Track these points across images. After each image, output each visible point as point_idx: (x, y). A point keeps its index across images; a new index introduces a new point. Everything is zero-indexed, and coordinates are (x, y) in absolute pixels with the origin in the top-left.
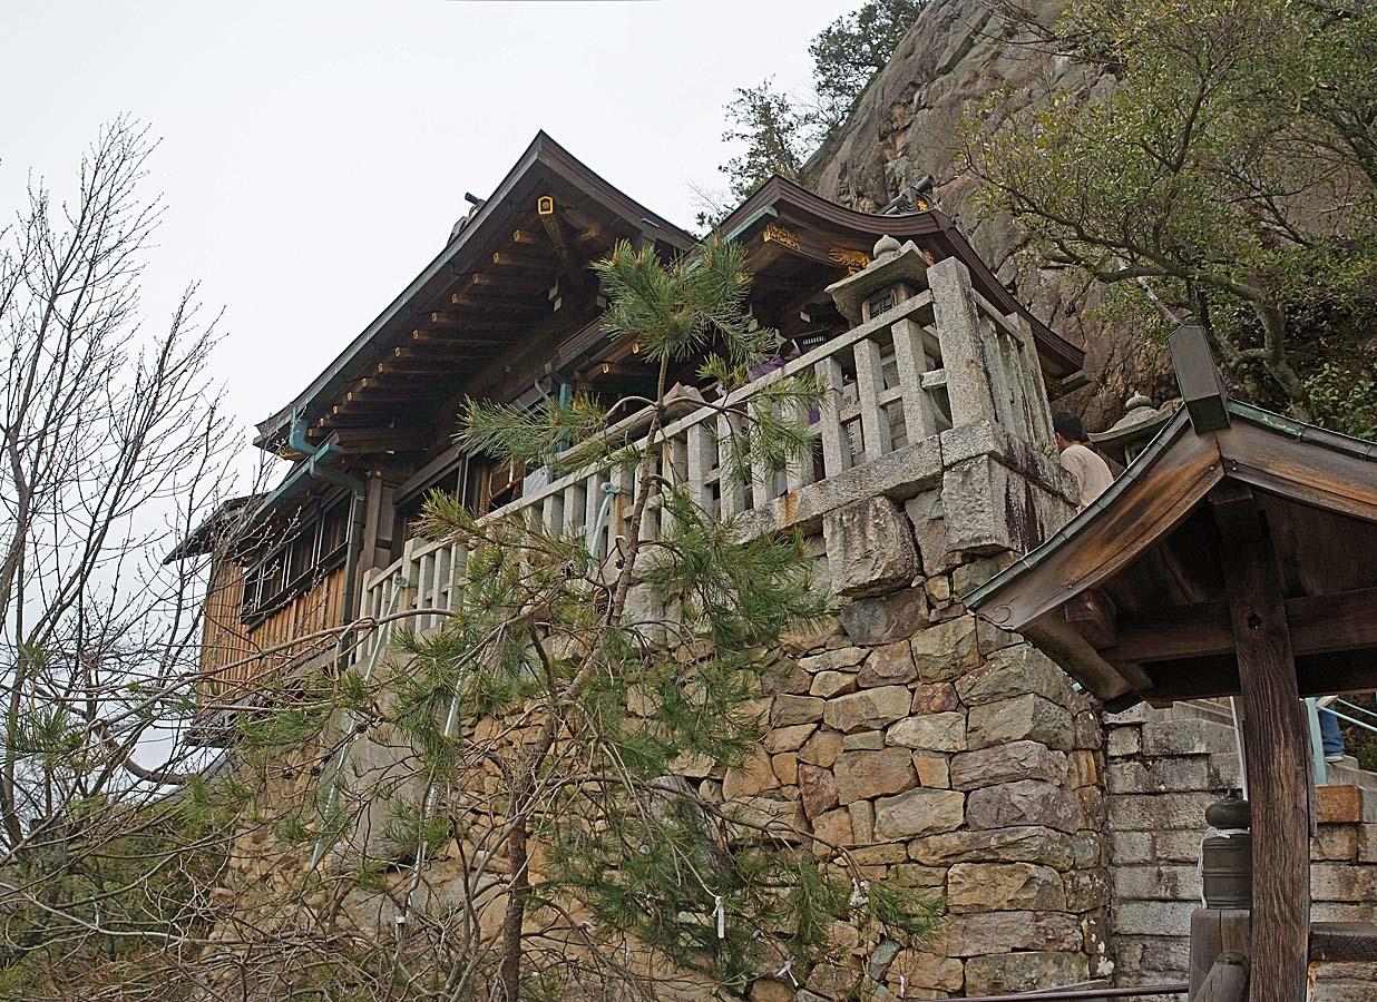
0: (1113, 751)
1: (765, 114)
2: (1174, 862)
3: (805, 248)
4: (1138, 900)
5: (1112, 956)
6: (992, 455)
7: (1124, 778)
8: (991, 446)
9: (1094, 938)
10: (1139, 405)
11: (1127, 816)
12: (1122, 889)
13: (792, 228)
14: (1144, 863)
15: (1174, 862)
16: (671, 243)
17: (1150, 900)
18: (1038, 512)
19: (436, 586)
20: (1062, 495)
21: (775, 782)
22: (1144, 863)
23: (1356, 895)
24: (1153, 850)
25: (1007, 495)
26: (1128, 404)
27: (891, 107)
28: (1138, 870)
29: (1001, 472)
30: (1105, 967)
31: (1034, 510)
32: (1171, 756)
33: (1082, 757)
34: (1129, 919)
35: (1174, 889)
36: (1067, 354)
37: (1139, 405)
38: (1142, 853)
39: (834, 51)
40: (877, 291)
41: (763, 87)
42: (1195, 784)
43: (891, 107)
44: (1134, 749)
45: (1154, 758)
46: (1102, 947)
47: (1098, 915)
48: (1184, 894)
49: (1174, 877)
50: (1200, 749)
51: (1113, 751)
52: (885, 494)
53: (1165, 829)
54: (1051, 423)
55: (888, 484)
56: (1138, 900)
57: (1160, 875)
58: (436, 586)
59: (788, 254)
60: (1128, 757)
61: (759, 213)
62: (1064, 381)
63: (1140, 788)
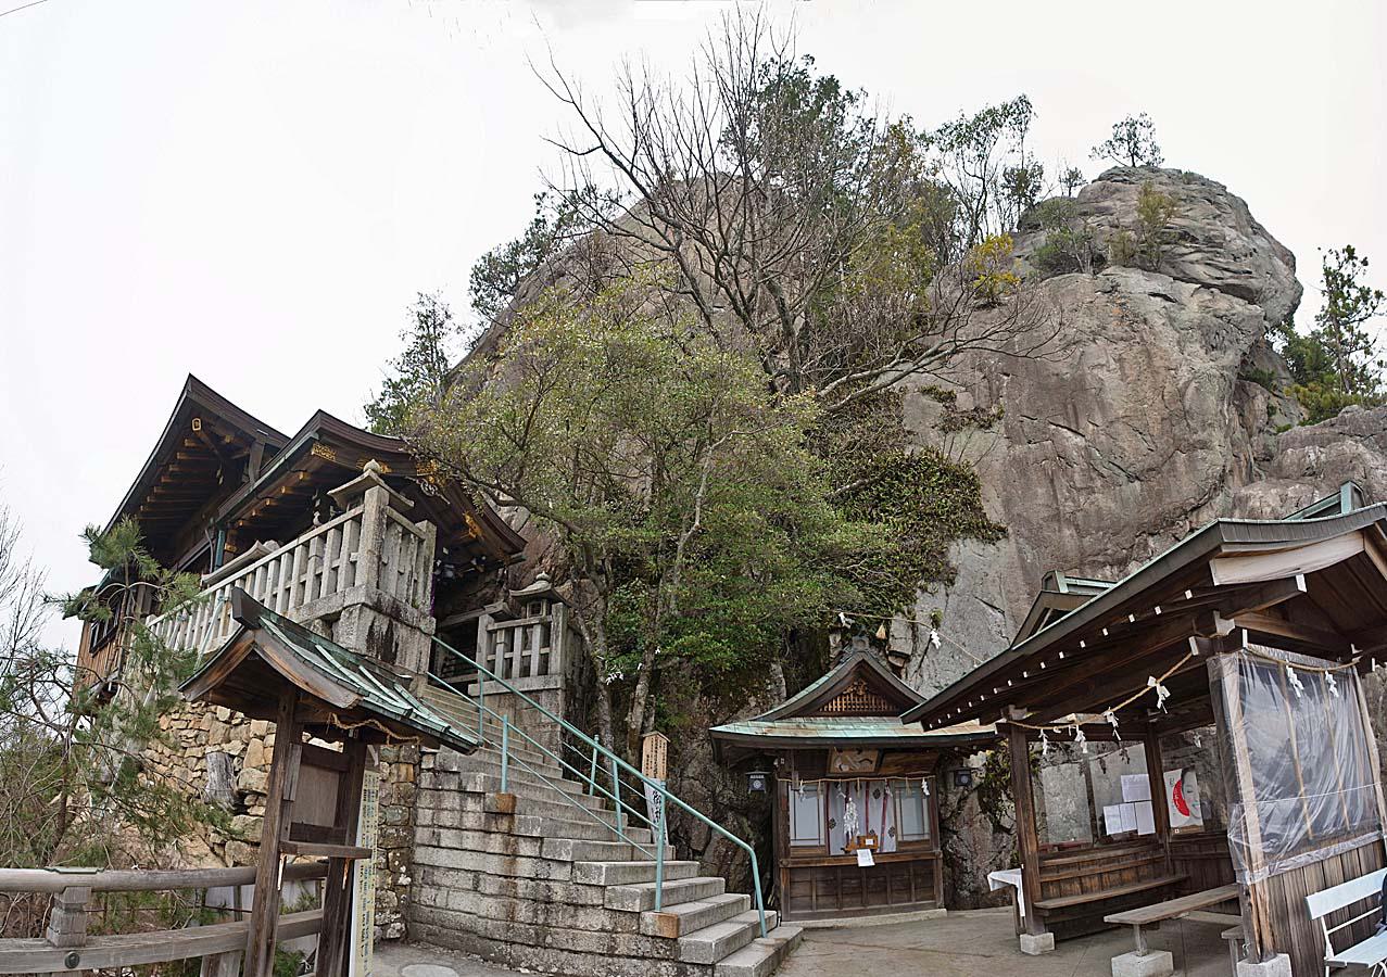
0: (423, 767)
1: (424, 319)
2: (441, 827)
3: (340, 459)
4: (424, 845)
5: (409, 874)
6: (363, 604)
7: (426, 780)
8: (363, 600)
9: (397, 863)
10: (541, 579)
11: (425, 801)
12: (418, 840)
13: (332, 446)
14: (428, 826)
15: (441, 827)
16: (274, 442)
17: (429, 846)
18: (395, 637)
19: (269, 588)
20: (419, 629)
21: (263, 762)
22: (428, 826)
23: (509, 853)
24: (433, 819)
25: (371, 627)
26: (538, 577)
27: (497, 338)
28: (425, 829)
29: (370, 615)
30: (404, 880)
31: (392, 634)
32: (445, 772)
33: (403, 768)
34: (421, 855)
35: (439, 842)
36: (515, 541)
37: (541, 579)
38: (428, 821)
39: (491, 275)
40: (355, 497)
41: (436, 294)
42: (452, 787)
43: (497, 338)
44: (431, 766)
45: (438, 772)
46: (403, 869)
47: (404, 851)
48: (443, 845)
49: (439, 835)
50: (455, 769)
51: (423, 767)
52: (320, 618)
53: (438, 809)
54: (429, 588)
55: (322, 613)
56: (424, 845)
57: (434, 833)
58: (269, 588)
59: (328, 463)
60: (429, 770)
61: (307, 437)
62: (513, 556)
63: (431, 787)
